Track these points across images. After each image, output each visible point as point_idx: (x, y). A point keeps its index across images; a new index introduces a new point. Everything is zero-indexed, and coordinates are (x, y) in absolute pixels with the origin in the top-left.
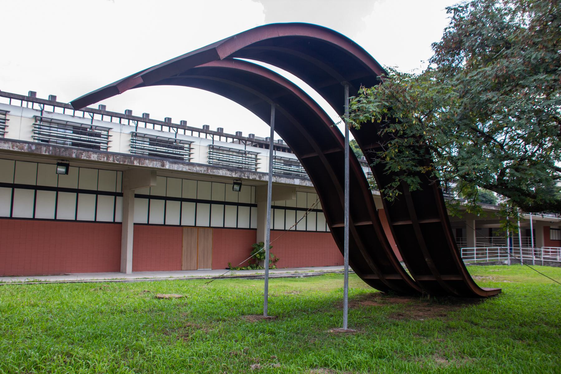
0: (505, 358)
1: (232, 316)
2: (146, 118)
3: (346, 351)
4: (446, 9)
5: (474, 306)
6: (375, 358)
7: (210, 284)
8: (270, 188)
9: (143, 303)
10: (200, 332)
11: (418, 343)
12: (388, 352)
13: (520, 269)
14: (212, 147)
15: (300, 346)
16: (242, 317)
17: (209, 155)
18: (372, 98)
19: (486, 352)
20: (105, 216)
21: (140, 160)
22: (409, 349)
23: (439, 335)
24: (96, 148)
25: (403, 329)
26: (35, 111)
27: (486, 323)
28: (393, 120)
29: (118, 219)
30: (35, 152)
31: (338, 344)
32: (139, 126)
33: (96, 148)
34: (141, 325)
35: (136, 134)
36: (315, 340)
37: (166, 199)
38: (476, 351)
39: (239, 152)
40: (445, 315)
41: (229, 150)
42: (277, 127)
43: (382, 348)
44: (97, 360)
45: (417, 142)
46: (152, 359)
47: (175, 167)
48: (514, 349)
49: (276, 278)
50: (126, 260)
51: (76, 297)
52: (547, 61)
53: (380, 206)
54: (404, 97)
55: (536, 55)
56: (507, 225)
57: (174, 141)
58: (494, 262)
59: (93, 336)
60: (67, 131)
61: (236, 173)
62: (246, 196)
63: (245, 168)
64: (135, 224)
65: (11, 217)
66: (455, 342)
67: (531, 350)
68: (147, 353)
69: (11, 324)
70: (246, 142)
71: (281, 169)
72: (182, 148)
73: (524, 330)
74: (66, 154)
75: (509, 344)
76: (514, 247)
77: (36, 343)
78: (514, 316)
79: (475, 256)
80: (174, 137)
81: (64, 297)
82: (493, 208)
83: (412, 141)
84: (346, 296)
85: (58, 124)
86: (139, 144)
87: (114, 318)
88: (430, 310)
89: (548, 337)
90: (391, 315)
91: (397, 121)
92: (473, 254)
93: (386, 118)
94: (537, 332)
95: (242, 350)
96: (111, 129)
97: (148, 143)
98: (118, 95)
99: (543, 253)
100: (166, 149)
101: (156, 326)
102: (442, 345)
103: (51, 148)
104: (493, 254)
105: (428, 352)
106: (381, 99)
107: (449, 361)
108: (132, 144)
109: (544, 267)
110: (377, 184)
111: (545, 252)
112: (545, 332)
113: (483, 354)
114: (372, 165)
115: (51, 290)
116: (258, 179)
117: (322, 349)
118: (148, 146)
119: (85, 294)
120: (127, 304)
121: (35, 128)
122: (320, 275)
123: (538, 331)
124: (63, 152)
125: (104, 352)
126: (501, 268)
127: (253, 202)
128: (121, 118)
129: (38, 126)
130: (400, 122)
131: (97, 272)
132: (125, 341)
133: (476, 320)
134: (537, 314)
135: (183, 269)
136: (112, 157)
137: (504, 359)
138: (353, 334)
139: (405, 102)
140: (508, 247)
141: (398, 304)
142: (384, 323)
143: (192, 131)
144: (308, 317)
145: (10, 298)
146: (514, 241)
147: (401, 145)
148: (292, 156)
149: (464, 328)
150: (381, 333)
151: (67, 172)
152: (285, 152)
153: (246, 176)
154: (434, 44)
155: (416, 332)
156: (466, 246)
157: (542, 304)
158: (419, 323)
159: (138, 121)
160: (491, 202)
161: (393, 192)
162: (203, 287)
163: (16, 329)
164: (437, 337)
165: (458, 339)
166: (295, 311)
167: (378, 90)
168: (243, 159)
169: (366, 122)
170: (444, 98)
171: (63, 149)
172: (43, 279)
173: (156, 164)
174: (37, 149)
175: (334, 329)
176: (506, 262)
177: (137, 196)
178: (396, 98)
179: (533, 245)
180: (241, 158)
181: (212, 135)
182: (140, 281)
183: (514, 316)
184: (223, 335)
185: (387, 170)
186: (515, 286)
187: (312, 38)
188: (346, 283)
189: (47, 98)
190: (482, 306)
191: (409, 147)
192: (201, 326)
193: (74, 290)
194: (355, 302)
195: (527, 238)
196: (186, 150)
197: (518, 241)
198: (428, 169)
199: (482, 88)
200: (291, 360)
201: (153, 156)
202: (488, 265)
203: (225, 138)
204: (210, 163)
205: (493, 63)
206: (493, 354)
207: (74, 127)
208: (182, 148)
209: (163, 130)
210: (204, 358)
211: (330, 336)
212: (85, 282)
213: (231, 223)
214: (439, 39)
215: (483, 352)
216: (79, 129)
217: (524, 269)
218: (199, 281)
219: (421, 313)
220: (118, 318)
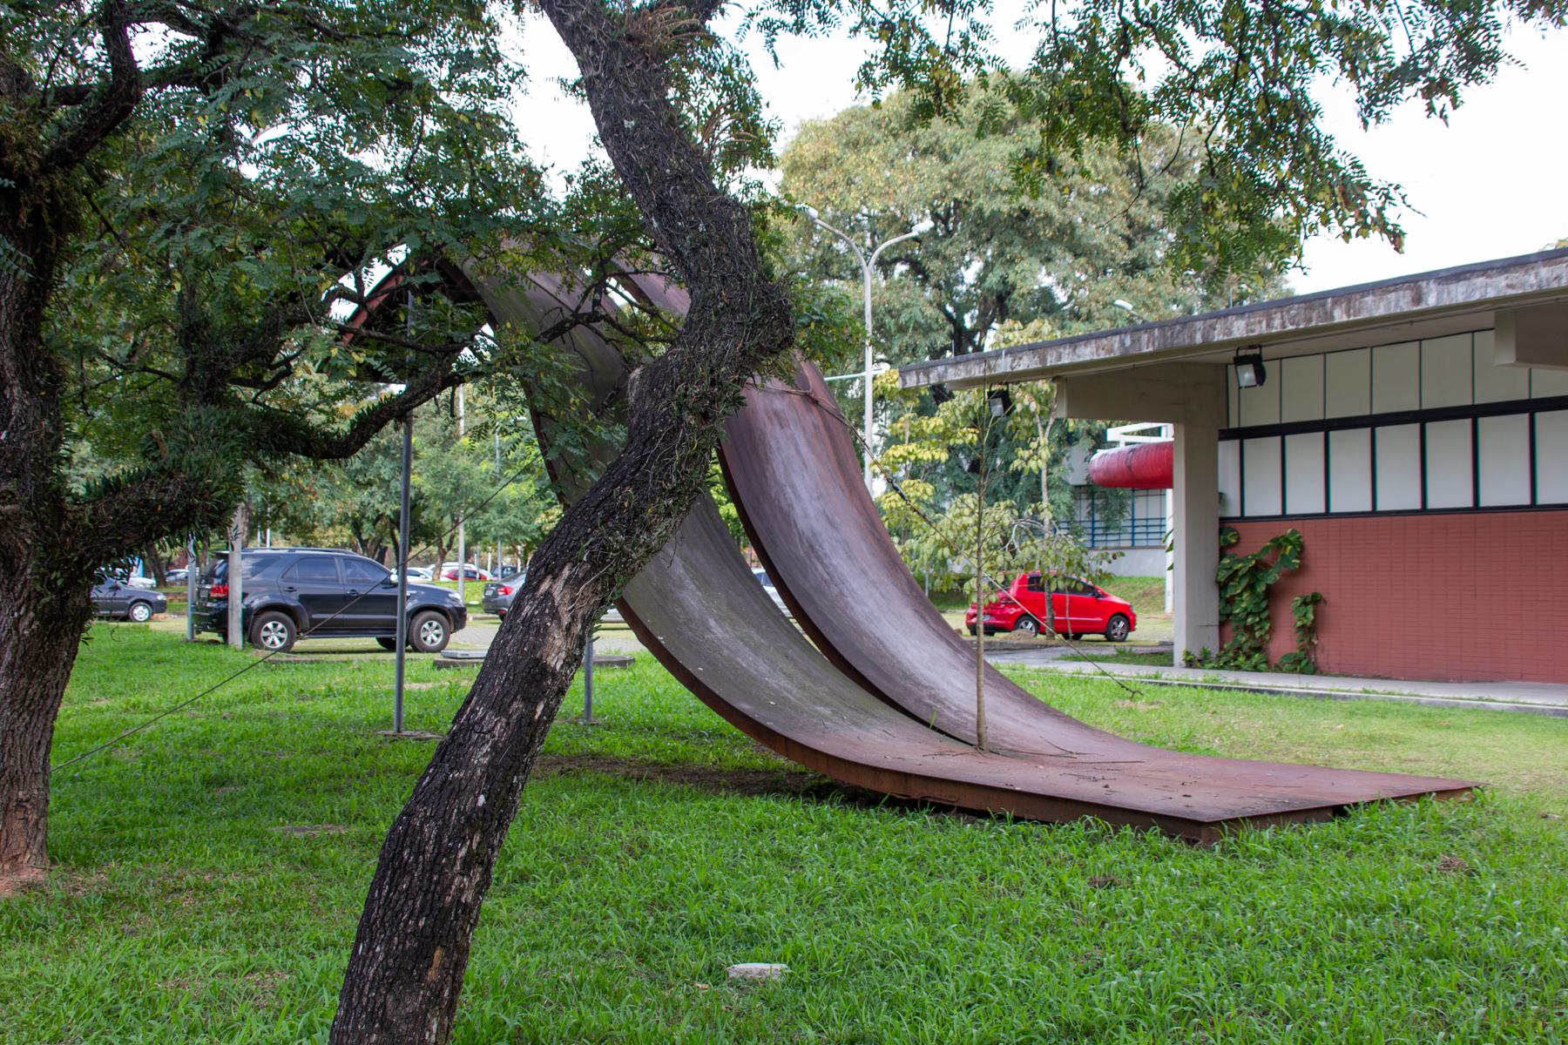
21: (1349, 302)
136: (1279, 315)
173: (1397, 301)
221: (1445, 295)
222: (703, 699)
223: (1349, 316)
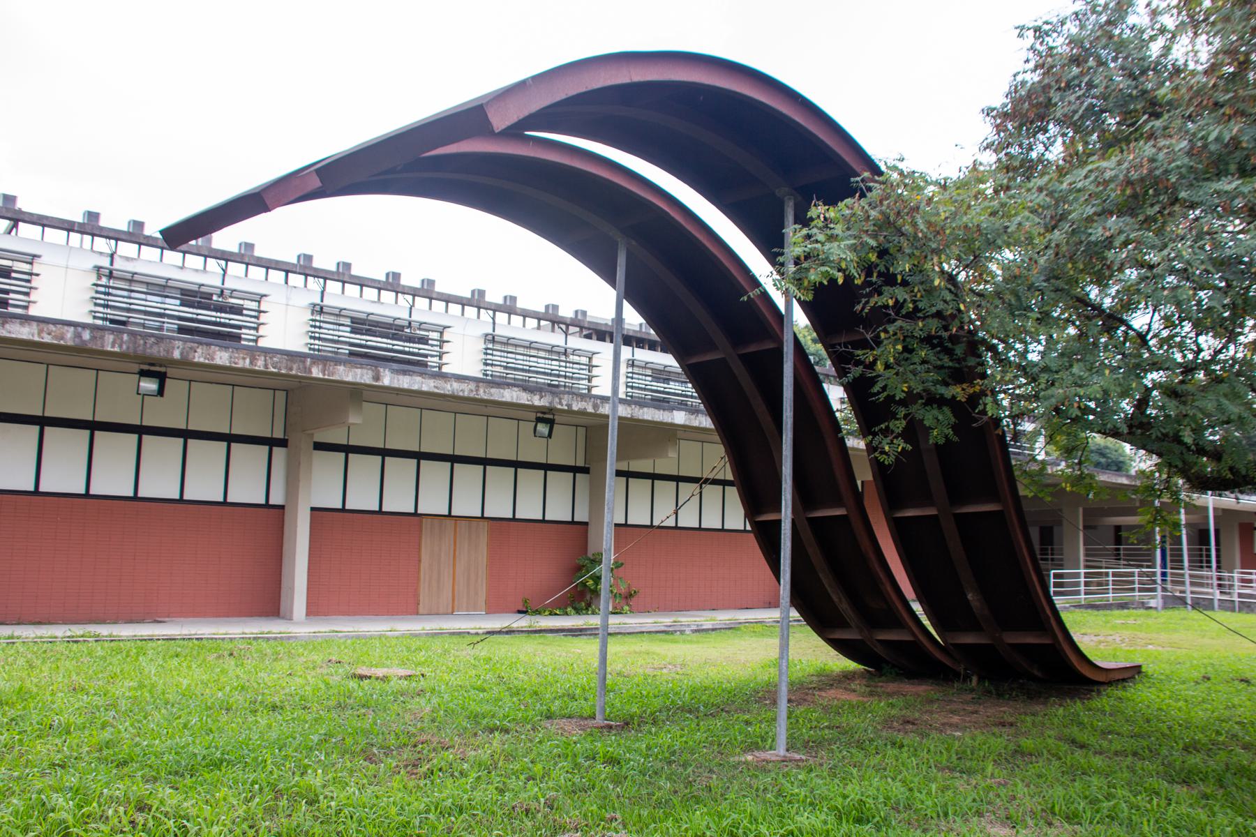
0: (1149, 825)
1: (526, 720)
2: (343, 275)
3: (780, 805)
4: (1016, 28)
5: (1079, 703)
6: (848, 821)
7: (479, 646)
8: (613, 429)
9: (323, 686)
10: (449, 756)
11: (947, 788)
12: (877, 809)
13: (1184, 619)
14: (491, 339)
15: (676, 792)
16: (546, 723)
17: (484, 357)
18: (838, 229)
19: (1106, 812)
20: (248, 490)
21: (325, 366)
22: (927, 803)
23: (997, 771)
24: (229, 338)
25: (915, 755)
26: (97, 256)
27: (1105, 744)
28: (890, 279)
29: (276, 499)
30: (90, 346)
31: (762, 787)
32: (328, 290)
33: (229, 338)
34: (315, 738)
35: (322, 308)
36: (711, 778)
37: (384, 453)
38: (1081, 808)
39: (552, 350)
40: (1011, 725)
41: (530, 345)
42: (635, 293)
43: (864, 798)
44: (205, 819)
45: (946, 328)
46: (334, 819)
47: (405, 382)
48: (1169, 804)
49: (628, 633)
50: (292, 589)
51: (174, 673)
52: (1244, 145)
53: (864, 474)
54: (914, 225)
55: (1220, 132)
56: (1155, 519)
57: (406, 323)
58: (1126, 603)
59: (204, 763)
60: (168, 300)
61: (541, 397)
62: (563, 449)
63: (565, 386)
64: (313, 509)
65: (36, 492)
66: (1032, 786)
67: (1211, 809)
68: (323, 803)
69: (20, 733)
70: (567, 328)
71: (645, 389)
72: (424, 340)
73: (1193, 761)
74: (157, 351)
75: (1157, 794)
76: (1172, 568)
77: (72, 780)
78: (1170, 728)
79: (1082, 588)
80: (407, 317)
81: (146, 671)
82: (1124, 481)
83: (934, 325)
84: (784, 678)
85: (148, 284)
86: (329, 332)
87: (256, 721)
88: (976, 712)
89: (1249, 779)
90: (888, 723)
91: (899, 281)
92: (1078, 584)
93: (875, 275)
94: (1224, 767)
95: (542, 800)
96: (265, 296)
97: (348, 329)
98: (263, 215)
99: (1236, 583)
100: (389, 341)
101: (349, 741)
102: (1002, 795)
103: (125, 337)
104: (1123, 583)
105: (970, 810)
106: (861, 231)
107: (1018, 832)
108: (313, 329)
109: (1240, 615)
110: (858, 423)
111: (1243, 581)
112: (1243, 767)
113: (1098, 816)
114: (845, 380)
115: (119, 657)
116: (590, 410)
117: (726, 799)
118: (348, 335)
119: (194, 666)
120: (287, 691)
121: (97, 292)
122: (730, 628)
123: (1227, 765)
124: (151, 347)
125: (225, 799)
126: (1139, 616)
127: (580, 463)
128: (287, 272)
129: (102, 289)
130: (905, 283)
131: (228, 617)
132: (275, 776)
133: (1082, 737)
134: (1224, 724)
135: (421, 610)
136: (263, 358)
137: (1146, 828)
138: (798, 767)
139: (915, 236)
140: (1158, 570)
141: (904, 696)
142: (871, 741)
143: (447, 302)
144: (698, 725)
145: (24, 674)
146: (1171, 555)
147: (910, 334)
148: (667, 360)
149: (1053, 755)
150: (862, 764)
151: (161, 392)
152: (655, 350)
153: (564, 402)
154: (988, 112)
155: (944, 762)
156: (1061, 566)
157: (1236, 701)
158: (950, 741)
159: (325, 279)
160: (1118, 466)
161: (892, 442)
162: (463, 653)
163: (31, 745)
164: (992, 774)
165: (1041, 781)
166: (669, 710)
167: (852, 209)
168: (560, 366)
169: (826, 283)
170: (1007, 227)
171: (153, 339)
172: (104, 630)
174: (93, 338)
175: (756, 753)
176: (1152, 603)
177: (319, 446)
178: (895, 227)
179: (1214, 564)
180: (557, 363)
181: (491, 313)
182: (322, 637)
183: (1170, 728)
184: (499, 765)
185: (879, 393)
186: (1172, 658)
187: (709, 86)
188: (784, 647)
189: (124, 228)
190: (1096, 703)
191: (928, 340)
192: (451, 743)
193: (172, 657)
194: (803, 692)
195: (1201, 550)
196: (432, 345)
197: (1181, 555)
198: (971, 391)
199: (1094, 209)
200: (653, 825)
201: (359, 356)
202: (1111, 609)
203: (460, 306)
204: (487, 375)
205: (1122, 152)
206: (1120, 815)
207: (184, 292)
208: (424, 340)
209: (382, 300)
210: (453, 819)
211: (745, 770)
212: (197, 639)
213: (529, 509)
214: (998, 100)
215: (1097, 812)
216: (194, 297)
217: (1193, 620)
218: (455, 639)
219: (955, 719)
220: (263, 723)
221: (396, 381)
222: (601, 654)
223: (324, 375)
